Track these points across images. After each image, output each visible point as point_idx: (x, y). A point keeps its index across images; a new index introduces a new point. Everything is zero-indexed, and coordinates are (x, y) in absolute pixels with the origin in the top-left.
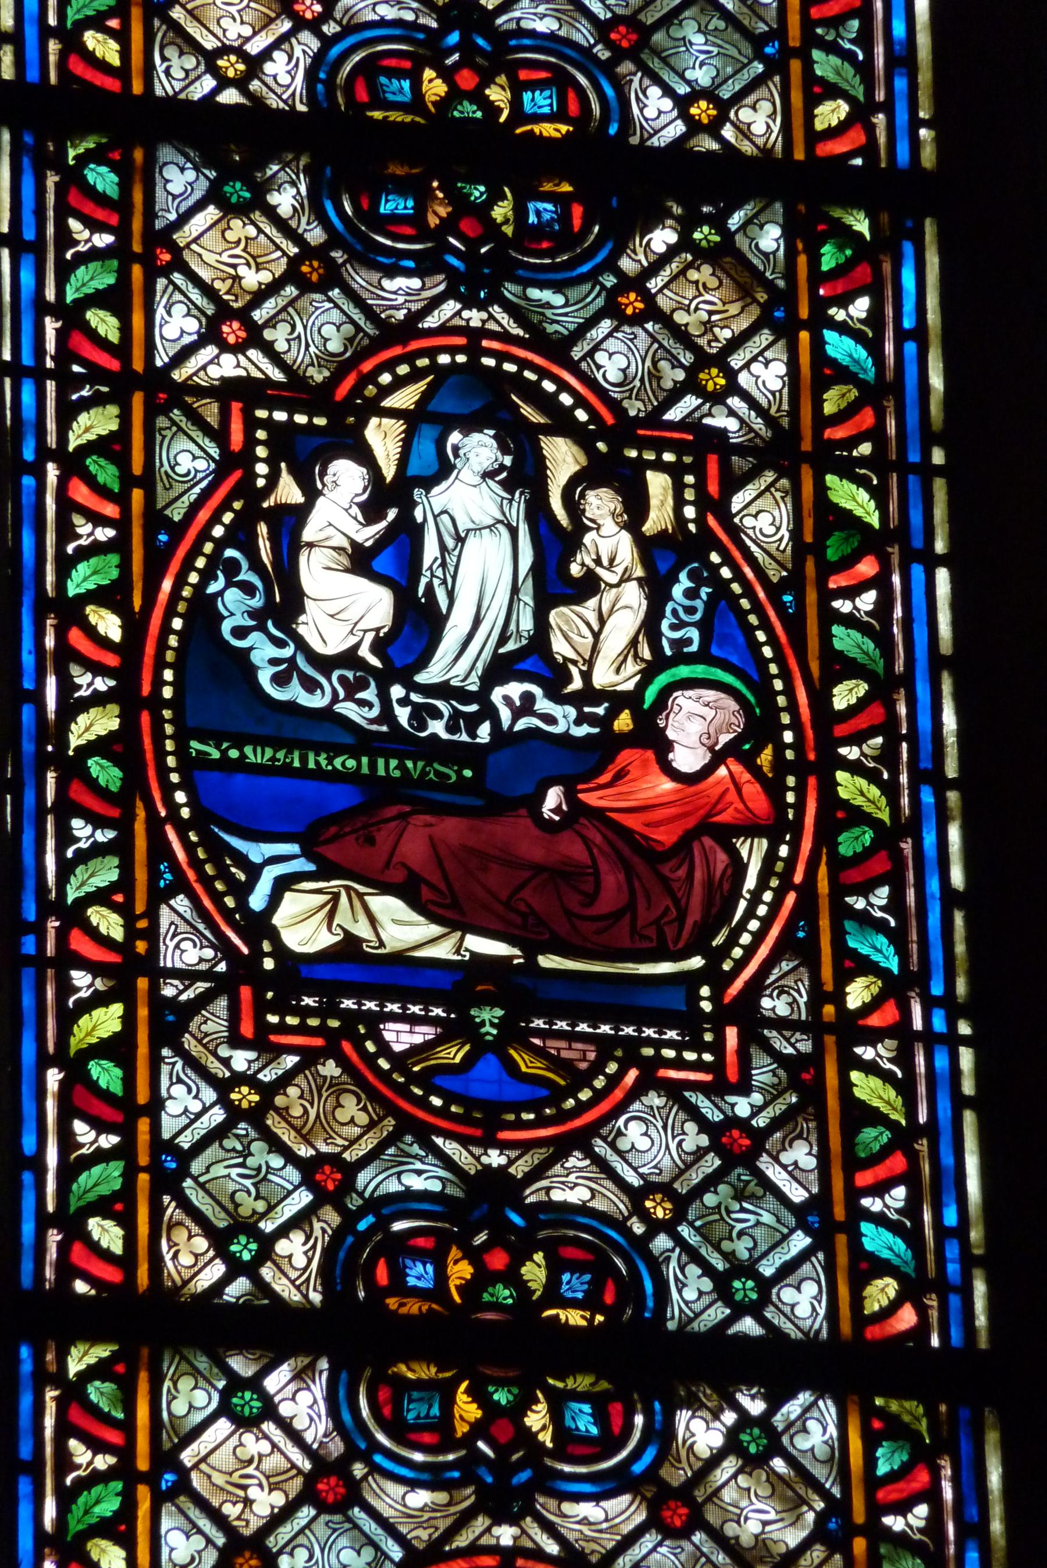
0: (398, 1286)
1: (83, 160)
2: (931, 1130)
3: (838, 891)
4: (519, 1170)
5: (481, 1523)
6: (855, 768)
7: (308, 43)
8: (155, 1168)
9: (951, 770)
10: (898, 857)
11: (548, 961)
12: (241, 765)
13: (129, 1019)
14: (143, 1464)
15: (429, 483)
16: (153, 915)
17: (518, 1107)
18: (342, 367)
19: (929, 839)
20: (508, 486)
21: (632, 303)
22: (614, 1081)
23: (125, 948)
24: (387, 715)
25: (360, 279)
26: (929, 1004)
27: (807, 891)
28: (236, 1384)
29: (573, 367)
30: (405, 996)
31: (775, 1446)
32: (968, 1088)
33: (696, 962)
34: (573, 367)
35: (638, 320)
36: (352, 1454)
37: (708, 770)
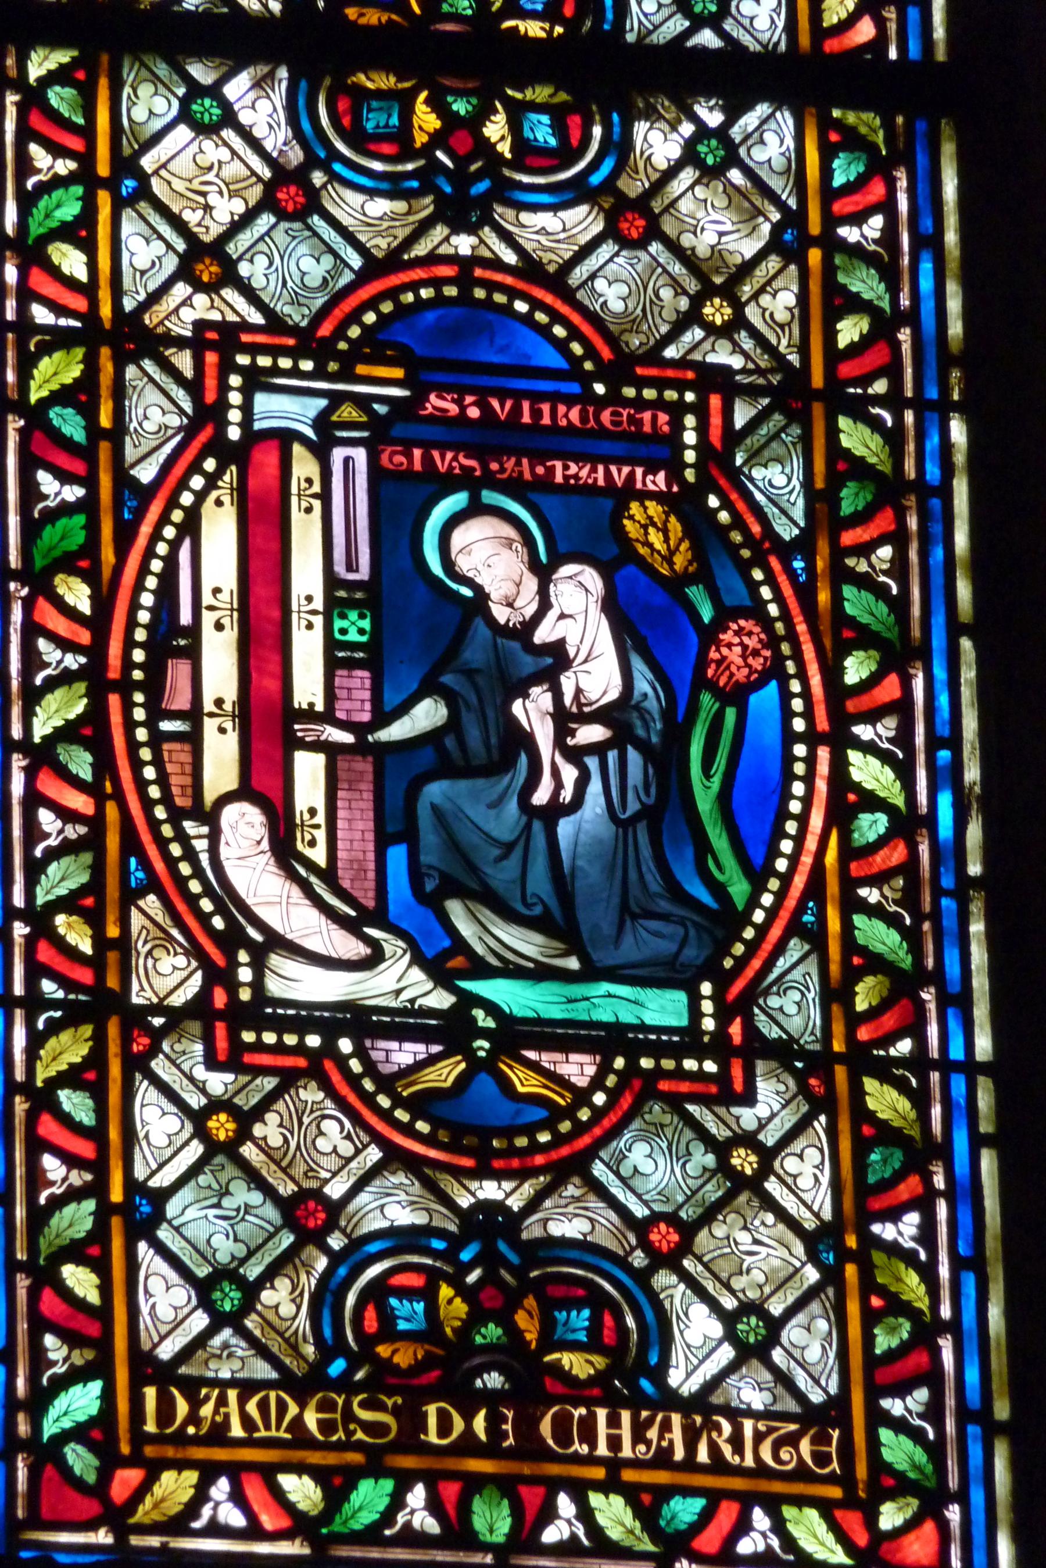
5: (440, 231)
14: (103, 170)
28: (195, 90)
31: (732, 158)
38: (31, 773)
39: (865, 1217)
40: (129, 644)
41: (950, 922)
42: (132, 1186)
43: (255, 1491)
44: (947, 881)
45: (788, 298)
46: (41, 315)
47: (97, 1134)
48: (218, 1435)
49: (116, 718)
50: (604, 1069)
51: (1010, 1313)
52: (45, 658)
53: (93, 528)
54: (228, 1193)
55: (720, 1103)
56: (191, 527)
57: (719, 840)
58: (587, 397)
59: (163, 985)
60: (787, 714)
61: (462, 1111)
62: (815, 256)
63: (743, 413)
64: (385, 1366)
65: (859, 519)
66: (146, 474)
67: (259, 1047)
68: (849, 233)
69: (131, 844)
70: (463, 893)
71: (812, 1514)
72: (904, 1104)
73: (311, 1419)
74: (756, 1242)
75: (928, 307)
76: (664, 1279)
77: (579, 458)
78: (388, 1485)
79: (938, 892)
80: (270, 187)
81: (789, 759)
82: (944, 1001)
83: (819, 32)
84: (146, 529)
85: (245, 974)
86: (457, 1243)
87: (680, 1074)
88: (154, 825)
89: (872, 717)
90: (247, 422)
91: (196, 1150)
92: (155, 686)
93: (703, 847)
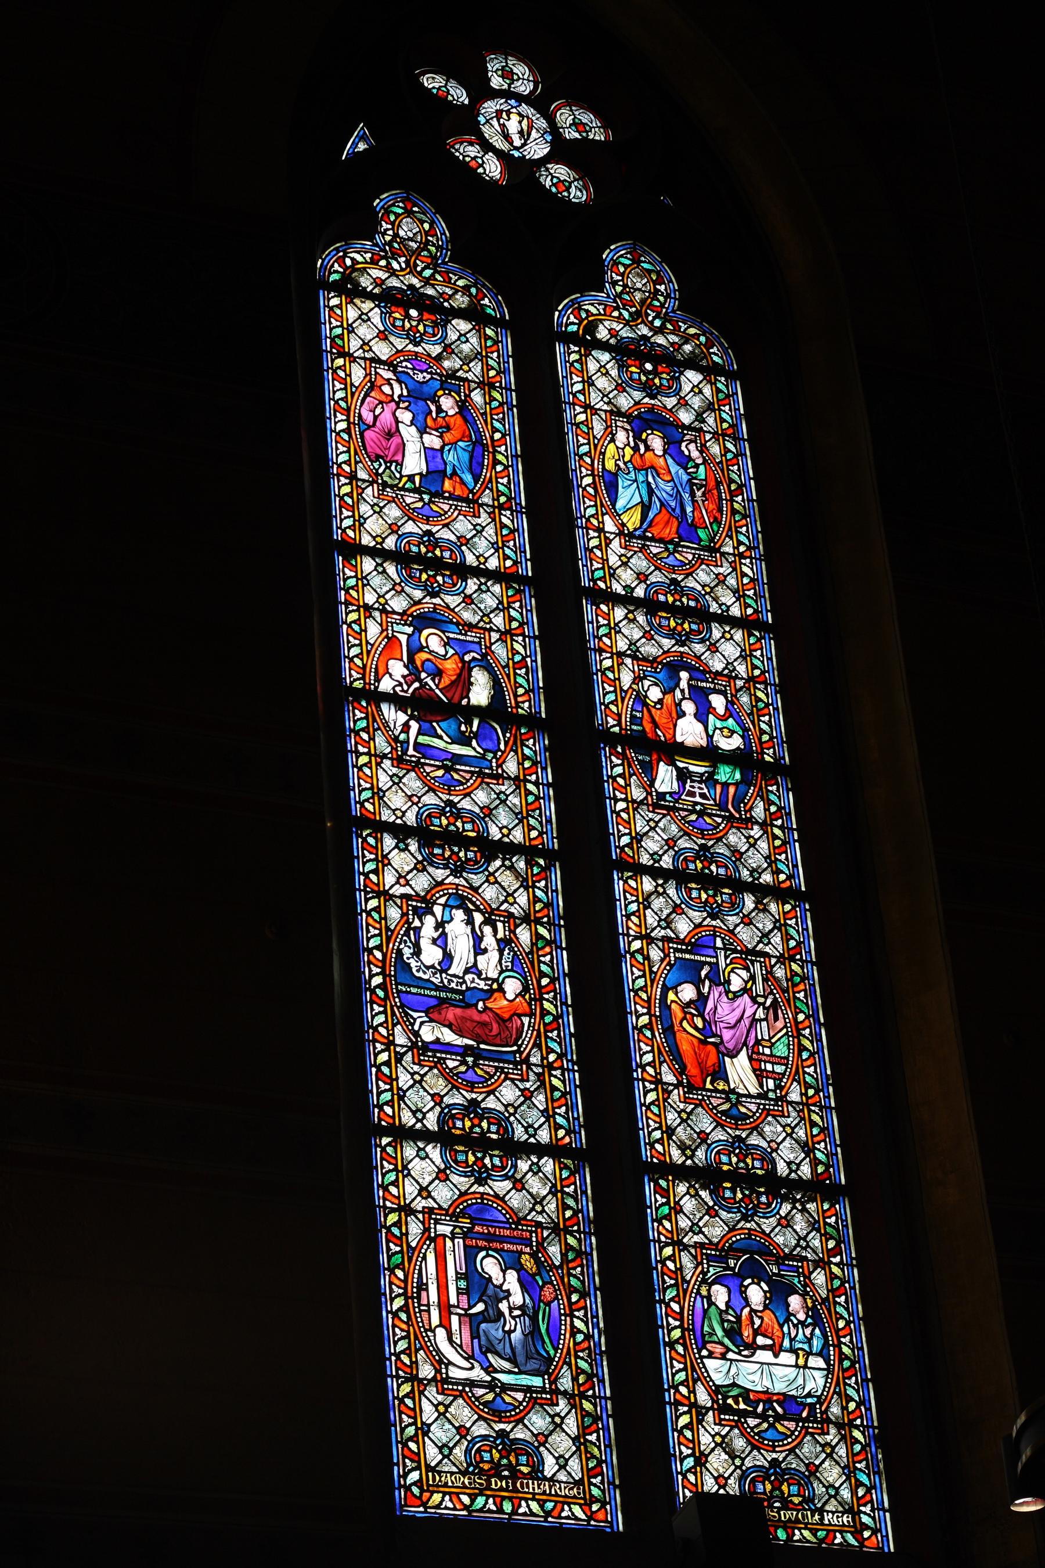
0: (454, 1127)
1: (367, 835)
2: (570, 1093)
3: (546, 1031)
4: (479, 1099)
5: (476, 1186)
6: (548, 1000)
7: (415, 809)
8: (398, 1094)
9: (569, 1002)
10: (558, 1023)
11: (482, 1046)
12: (410, 992)
13: (390, 1056)
14: (400, 1168)
15: (448, 922)
16: (393, 1030)
17: (478, 1083)
18: (428, 892)
19: (566, 1019)
20: (467, 924)
21: (492, 879)
22: (499, 1077)
23: (387, 1038)
24: (442, 982)
25: (430, 869)
26: (568, 1061)
27: (539, 1030)
28: (420, 1149)
29: (479, 895)
30: (452, 1054)
31: (540, 1170)
32: (578, 1083)
33: (515, 1048)
34: (479, 895)
35: (493, 884)
36: (446, 1168)
37: (515, 999)
38: (393, 1319)
39: (585, 1435)
40: (413, 1287)
41: (599, 1362)
42: (423, 1423)
43: (454, 1499)
44: (598, 1352)
45: (554, 1205)
46: (388, 1204)
47: (414, 1410)
48: (446, 1485)
49: (411, 1306)
50: (525, 1397)
51: (618, 1458)
53: (403, 1257)
56: (424, 1258)
57: (547, 1340)
58: (510, 1228)
59: (426, 1373)
60: (560, 1309)
61: (494, 1406)
62: (559, 1195)
63: (546, 1233)
64: (482, 1469)
65: (573, 1260)
66: (413, 1244)
67: (448, 1389)
68: (566, 1190)
69: (416, 1338)
70: (491, 1352)
71: (577, 1507)
72: (591, 1407)
73: (466, 1481)
75: (585, 1208)
76: (542, 1449)
77: (510, 1243)
78: (484, 1498)
79: (596, 1354)
80: (437, 1173)
81: (561, 1320)
82: (599, 1381)
83: (557, 1140)
84: (414, 1258)
85: (444, 1371)
86: (496, 1439)
87: (542, 1398)
88: (421, 1333)
89: (578, 1310)
90: (435, 1232)
91: (436, 1414)
92: (419, 1298)
93: (544, 1342)
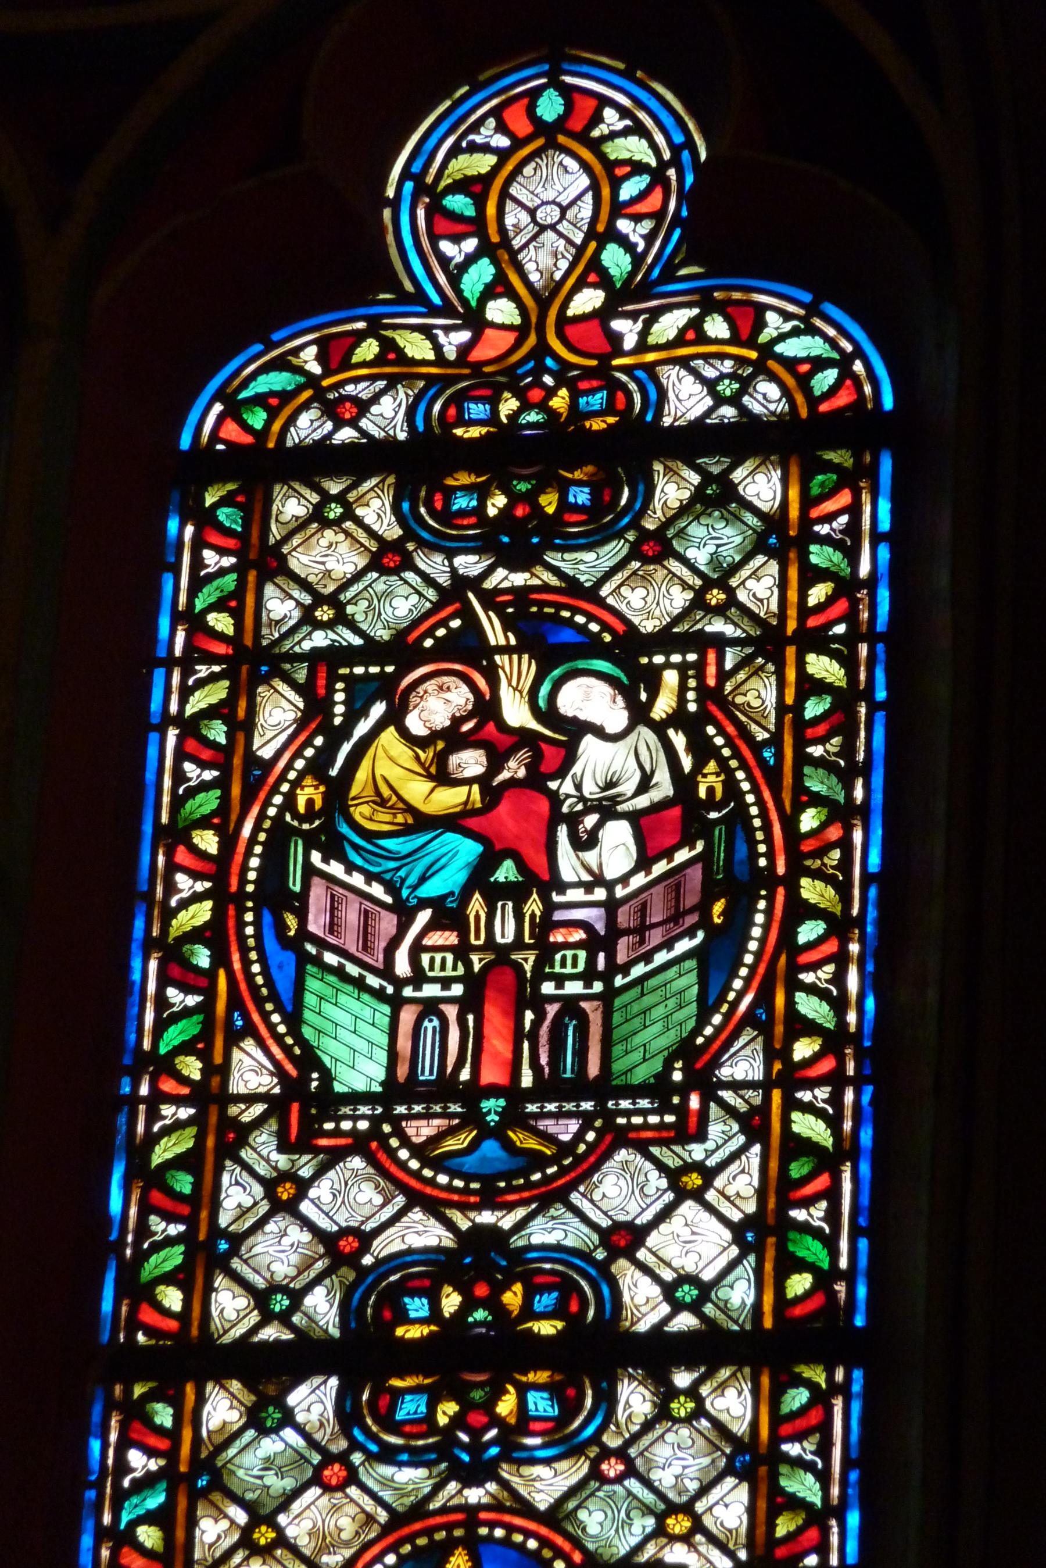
5: (453, 1486)
39: (786, 1203)
52: (153, 1228)
54: (286, 1234)
55: (676, 1143)
74: (693, 1233)
